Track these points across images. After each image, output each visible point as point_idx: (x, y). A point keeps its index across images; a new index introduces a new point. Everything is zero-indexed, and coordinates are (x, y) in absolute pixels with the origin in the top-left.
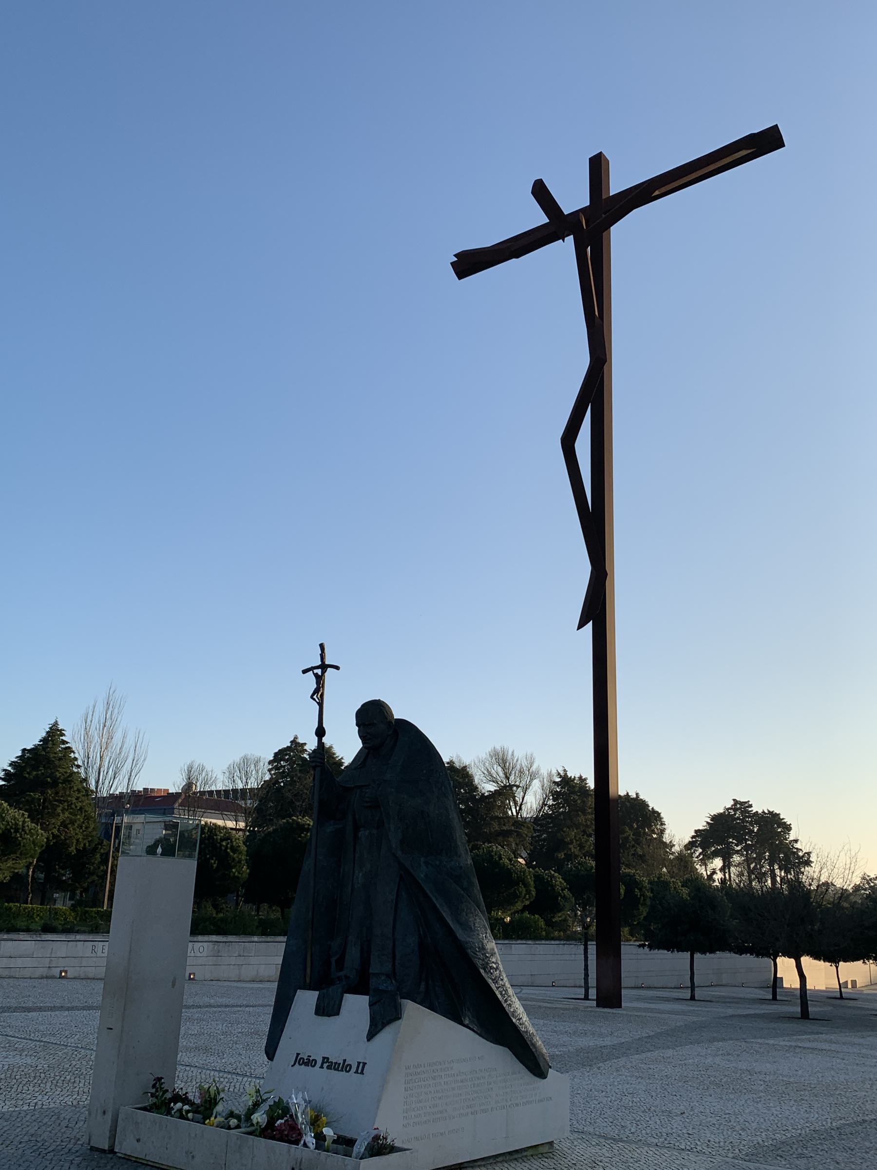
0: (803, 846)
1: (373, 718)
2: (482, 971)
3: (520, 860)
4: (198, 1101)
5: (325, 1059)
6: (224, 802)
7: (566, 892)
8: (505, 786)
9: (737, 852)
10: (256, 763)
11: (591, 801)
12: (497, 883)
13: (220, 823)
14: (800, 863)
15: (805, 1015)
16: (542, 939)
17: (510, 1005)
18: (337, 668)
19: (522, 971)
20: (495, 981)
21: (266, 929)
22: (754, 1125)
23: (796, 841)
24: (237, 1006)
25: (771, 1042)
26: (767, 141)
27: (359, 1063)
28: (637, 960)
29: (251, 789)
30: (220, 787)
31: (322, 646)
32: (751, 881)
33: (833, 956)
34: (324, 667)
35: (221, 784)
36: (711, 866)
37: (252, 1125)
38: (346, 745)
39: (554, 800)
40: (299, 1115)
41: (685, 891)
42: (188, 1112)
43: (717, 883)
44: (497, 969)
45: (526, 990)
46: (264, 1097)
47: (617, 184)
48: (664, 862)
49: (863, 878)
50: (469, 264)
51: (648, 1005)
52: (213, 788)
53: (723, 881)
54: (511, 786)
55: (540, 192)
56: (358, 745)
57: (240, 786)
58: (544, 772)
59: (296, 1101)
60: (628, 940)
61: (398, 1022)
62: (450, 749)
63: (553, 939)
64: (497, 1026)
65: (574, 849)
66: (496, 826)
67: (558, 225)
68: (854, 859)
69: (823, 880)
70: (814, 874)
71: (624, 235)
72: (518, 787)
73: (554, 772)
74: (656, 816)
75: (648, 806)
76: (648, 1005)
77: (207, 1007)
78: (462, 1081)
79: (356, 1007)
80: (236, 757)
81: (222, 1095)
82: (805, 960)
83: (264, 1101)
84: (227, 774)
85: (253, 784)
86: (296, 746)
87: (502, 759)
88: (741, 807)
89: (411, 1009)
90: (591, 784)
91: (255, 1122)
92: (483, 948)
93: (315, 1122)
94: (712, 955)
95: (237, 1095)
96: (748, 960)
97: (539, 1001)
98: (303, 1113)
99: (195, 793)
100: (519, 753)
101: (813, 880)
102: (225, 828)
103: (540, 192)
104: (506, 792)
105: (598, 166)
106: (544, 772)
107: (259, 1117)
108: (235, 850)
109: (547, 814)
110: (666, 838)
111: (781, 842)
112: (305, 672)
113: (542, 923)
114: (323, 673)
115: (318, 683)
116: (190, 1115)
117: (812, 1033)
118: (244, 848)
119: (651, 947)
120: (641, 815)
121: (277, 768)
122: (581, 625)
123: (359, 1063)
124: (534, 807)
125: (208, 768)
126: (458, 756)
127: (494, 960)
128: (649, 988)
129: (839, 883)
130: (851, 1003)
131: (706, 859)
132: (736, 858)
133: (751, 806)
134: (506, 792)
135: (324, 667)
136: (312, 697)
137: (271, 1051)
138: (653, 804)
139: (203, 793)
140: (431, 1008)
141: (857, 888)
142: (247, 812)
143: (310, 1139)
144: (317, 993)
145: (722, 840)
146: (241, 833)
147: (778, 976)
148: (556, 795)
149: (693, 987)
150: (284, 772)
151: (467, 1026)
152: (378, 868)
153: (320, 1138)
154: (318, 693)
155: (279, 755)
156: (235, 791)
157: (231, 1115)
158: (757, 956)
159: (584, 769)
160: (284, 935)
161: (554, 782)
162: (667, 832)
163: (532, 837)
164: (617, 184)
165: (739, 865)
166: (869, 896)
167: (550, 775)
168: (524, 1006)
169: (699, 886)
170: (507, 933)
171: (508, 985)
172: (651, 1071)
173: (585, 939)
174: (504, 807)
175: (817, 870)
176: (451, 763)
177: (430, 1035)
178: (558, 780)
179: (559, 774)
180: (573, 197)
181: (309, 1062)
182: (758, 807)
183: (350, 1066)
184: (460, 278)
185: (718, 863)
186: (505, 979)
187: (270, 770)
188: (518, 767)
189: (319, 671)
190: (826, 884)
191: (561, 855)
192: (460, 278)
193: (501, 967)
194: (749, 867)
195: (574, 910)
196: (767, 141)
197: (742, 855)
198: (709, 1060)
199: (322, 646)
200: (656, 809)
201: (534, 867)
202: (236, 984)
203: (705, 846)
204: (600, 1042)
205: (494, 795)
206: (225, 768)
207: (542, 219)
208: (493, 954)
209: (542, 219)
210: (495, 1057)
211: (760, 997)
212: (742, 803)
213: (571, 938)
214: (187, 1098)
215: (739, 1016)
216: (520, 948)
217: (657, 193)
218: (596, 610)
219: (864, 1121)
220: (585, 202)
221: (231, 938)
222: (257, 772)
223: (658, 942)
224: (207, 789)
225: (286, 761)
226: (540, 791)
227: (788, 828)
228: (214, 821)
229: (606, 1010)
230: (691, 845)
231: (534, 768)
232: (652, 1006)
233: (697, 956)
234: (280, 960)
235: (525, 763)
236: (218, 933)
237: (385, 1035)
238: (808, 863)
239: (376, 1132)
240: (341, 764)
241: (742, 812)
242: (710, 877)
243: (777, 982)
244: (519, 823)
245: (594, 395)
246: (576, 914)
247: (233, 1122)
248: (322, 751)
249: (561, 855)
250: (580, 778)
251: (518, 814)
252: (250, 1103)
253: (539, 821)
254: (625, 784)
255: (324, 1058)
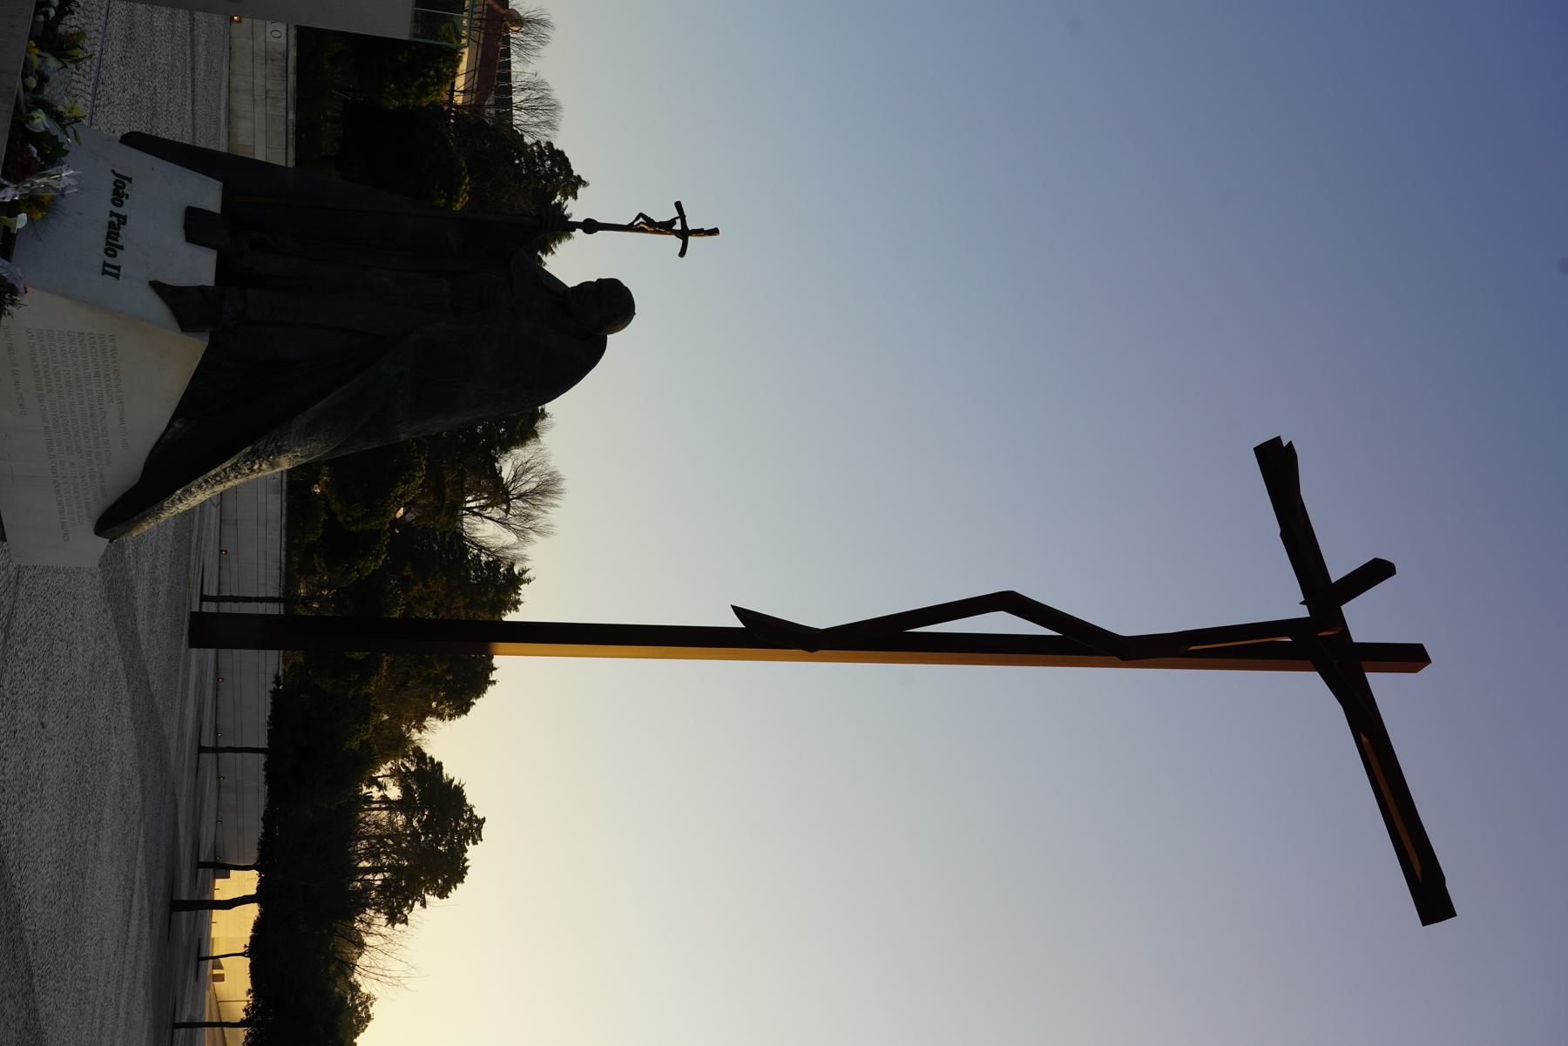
0: (417, 914)
1: (609, 304)
2: (249, 449)
3: (401, 511)
4: (61, 29)
5: (123, 220)
6: (495, 74)
7: (355, 575)
8: (508, 493)
9: (409, 821)
10: (548, 124)
11: (484, 616)
12: (365, 477)
13: (463, 67)
14: (391, 908)
15: (176, 906)
16: (288, 536)
17: (200, 487)
18: (682, 253)
19: (243, 509)
20: (235, 468)
21: (305, 133)
22: (26, 824)
23: (424, 904)
24: (193, 86)
25: (140, 857)
26: (1433, 903)
27: (118, 268)
28: (257, 673)
29: (511, 115)
30: (516, 68)
31: (714, 232)
32: (368, 838)
33: (259, 949)
34: (684, 234)
35: (521, 69)
36: (389, 783)
37: (29, 111)
38: (570, 263)
39: (488, 563)
40: (45, 179)
41: (355, 745)
42: (46, 14)
43: (365, 790)
44: (252, 470)
45: (215, 511)
46: (69, 130)
47: (1381, 684)
48: (397, 717)
49: (368, 997)
50: (1277, 463)
51: (192, 685)
52: (514, 58)
53: (368, 799)
54: (507, 501)
55: (1378, 571)
56: (571, 282)
57: (516, 99)
58: (528, 550)
59: (66, 175)
60: (285, 661)
61: (175, 325)
62: (565, 413)
63: (288, 556)
64: (174, 463)
65: (415, 590)
66: (450, 477)
67: (1326, 594)
68: (396, 982)
69: (368, 940)
70: (377, 931)
71: (1307, 691)
72: (507, 511)
73: (527, 565)
74: (463, 708)
75: (478, 697)
76: (192, 685)
77: (192, 41)
78: (92, 415)
79: (198, 267)
80: (558, 94)
81: (72, 66)
82: (253, 911)
83: (63, 128)
84: (534, 80)
85: (519, 118)
86: (573, 184)
87: (546, 489)
88: (474, 829)
89: (191, 350)
90: (510, 617)
91: (35, 114)
92: (280, 451)
93: (33, 203)
94: (262, 779)
95: (72, 89)
96: (254, 830)
97: (200, 530)
98: (47, 186)
99: (507, 30)
100: (554, 514)
101: (369, 925)
102: (455, 75)
103: (1378, 571)
104: (499, 494)
105: (1410, 657)
106: (528, 550)
107: (40, 120)
108: (423, 90)
109: (467, 552)
110: (431, 722)
111: (424, 883)
112: (678, 205)
113: (311, 538)
114: (676, 233)
115: (661, 224)
116: (41, 18)
117: (151, 912)
118: (425, 102)
119: (275, 693)
120: (462, 687)
121: (541, 153)
122: (738, 611)
123: (118, 268)
124: (478, 534)
125: (544, 51)
126: (552, 425)
127: (264, 466)
128: (217, 689)
129: (363, 961)
130: (191, 972)
131: (400, 777)
132: (400, 819)
133: (475, 843)
134: (499, 494)
135: (684, 234)
136: (641, 215)
137: (134, 140)
138: (480, 705)
139: (507, 41)
140: (197, 375)
141: (355, 988)
142: (476, 108)
143: (10, 194)
144: (1368, 675)
145: (426, 801)
146: (446, 98)
147: (232, 872)
148: (494, 566)
149: (217, 750)
150: (535, 164)
151: (170, 425)
152: (399, 302)
153: (13, 209)
154: (645, 225)
155: (560, 159)
156: (509, 90)
157: (43, 80)
158: (260, 843)
159: (531, 607)
160: (296, 160)
161: (512, 565)
162: (439, 723)
163: (434, 530)
164: (1381, 684)
165: (391, 822)
166: (344, 1000)
167: (523, 558)
168: (192, 511)
169: (362, 768)
170: (297, 483)
171: (229, 484)
172: (100, 684)
173: (288, 598)
174: (477, 491)
175: (383, 930)
176: (543, 415)
177: (155, 374)
178: (516, 570)
179: (525, 572)
180: (1366, 619)
181: (118, 197)
182: (473, 852)
183: (114, 256)
184: (1258, 450)
185: (394, 793)
186: (236, 482)
187: (538, 143)
188: (535, 513)
189: (678, 226)
190: (361, 945)
191: (407, 571)
192: (1258, 450)
193: (254, 476)
194: (388, 836)
195: (328, 586)
196: (1433, 903)
197: (405, 827)
198: (115, 767)
199: (714, 232)
200: (473, 709)
201: (391, 530)
202: (224, 84)
203: (420, 775)
204: (142, 615)
205: (496, 476)
206: (543, 76)
207: (1338, 568)
208: (272, 465)
209: (1338, 568)
210: (125, 459)
211: (203, 843)
212: (479, 830)
213: (290, 577)
214: (66, 13)
215: (176, 814)
216: (274, 506)
217: (1365, 740)
218: (760, 634)
219: (31, 976)
220: (1357, 638)
221: (292, 78)
222: (536, 125)
223: (280, 702)
224: (513, 48)
225: (552, 168)
226: (500, 543)
227: (442, 893)
228: (465, 58)
229: (186, 626)
230: (420, 755)
231: (533, 536)
232: (191, 692)
233: (262, 758)
234: (260, 156)
235: (541, 522)
236: (298, 59)
237: (157, 308)
238: (392, 920)
239: (20, 287)
240: (545, 252)
241: (466, 830)
242: (374, 782)
243: (223, 870)
244: (454, 511)
245: (1073, 641)
246: (323, 588)
247: (33, 82)
248: (564, 227)
249: (407, 571)
250: (519, 602)
251: (469, 509)
252: (60, 108)
253: (458, 542)
254: (509, 666)
255: (125, 218)
